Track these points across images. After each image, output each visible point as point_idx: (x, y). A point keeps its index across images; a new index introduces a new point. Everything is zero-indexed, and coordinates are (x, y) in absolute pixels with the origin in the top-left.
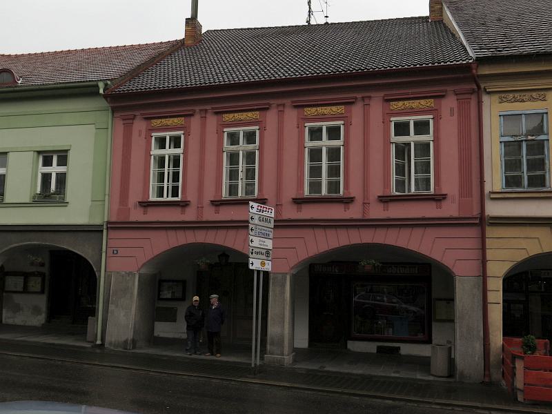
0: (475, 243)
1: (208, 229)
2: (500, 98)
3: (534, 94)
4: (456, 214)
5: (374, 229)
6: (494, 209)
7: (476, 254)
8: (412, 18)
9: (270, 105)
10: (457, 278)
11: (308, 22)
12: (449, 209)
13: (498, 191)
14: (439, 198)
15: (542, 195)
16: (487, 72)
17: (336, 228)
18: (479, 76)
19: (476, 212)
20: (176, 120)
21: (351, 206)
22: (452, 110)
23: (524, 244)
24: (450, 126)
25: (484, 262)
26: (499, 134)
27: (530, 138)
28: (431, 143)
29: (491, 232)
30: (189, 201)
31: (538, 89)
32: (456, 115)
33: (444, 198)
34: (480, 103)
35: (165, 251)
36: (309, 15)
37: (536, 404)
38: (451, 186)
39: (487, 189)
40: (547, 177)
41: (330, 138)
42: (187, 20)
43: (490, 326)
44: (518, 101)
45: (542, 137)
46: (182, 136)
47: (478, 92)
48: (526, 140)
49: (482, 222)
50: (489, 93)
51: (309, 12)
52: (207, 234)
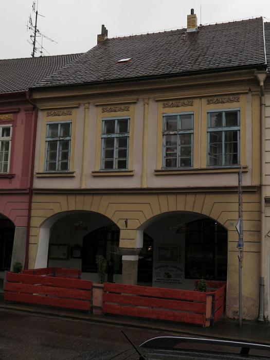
0: (26, 206)
1: (85, 195)
2: (164, 104)
3: (186, 101)
4: (18, 187)
5: (83, 196)
6: (39, 184)
7: (25, 213)
8: (13, 59)
9: (20, 109)
10: (16, 228)
11: (33, 55)
12: (16, 184)
13: (41, 172)
14: (11, 177)
15: (191, 172)
16: (38, 97)
17: (158, 195)
18: (36, 100)
19: (29, 186)
20: (7, 116)
21: (13, 180)
22: (22, 120)
23: (51, 206)
24: (21, 130)
25: (29, 217)
26: (45, 136)
27: (61, 139)
28: (10, 141)
29: (36, 198)
30: (14, 175)
31: (120, 104)
32: (24, 124)
33: (13, 177)
34: (36, 116)
35: (173, 212)
36: (34, 50)
37: (107, 315)
38: (18, 171)
39: (36, 170)
40: (238, 155)
41: (228, 125)
42: (98, 36)
43: (30, 259)
44: (220, 103)
45: (68, 138)
46: (11, 127)
47: (35, 109)
48: (59, 140)
49: (31, 192)
50: (42, 110)
51: (34, 48)
52: (93, 198)
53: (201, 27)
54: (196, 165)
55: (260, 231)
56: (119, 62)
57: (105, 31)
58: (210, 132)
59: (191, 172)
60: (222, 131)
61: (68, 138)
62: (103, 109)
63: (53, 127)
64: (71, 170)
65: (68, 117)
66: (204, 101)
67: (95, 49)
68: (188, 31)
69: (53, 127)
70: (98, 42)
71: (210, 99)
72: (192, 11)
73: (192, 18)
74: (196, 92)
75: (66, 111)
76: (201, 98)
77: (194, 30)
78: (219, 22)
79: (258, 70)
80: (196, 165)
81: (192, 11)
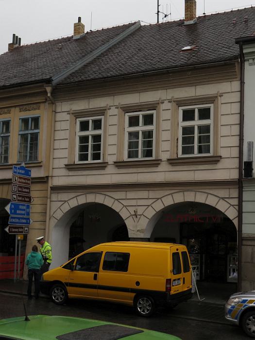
15: (7, 167)
26: (18, 130)
53: (205, 18)
54: (10, 162)
55: (45, 221)
56: (183, 50)
57: (16, 40)
58: (21, 135)
59: (7, 167)
60: (28, 134)
61: (9, 134)
62: (20, 109)
63: (25, 121)
64: (40, 160)
65: (37, 111)
66: (18, 109)
67: (5, 54)
68: (73, 38)
69: (25, 121)
70: (9, 49)
71: (22, 108)
72: (80, 19)
73: (78, 26)
74: (13, 102)
75: (6, 110)
76: (15, 106)
77: (192, 22)
78: (105, 27)
79: (47, 84)
80: (10, 162)
81: (80, 19)
